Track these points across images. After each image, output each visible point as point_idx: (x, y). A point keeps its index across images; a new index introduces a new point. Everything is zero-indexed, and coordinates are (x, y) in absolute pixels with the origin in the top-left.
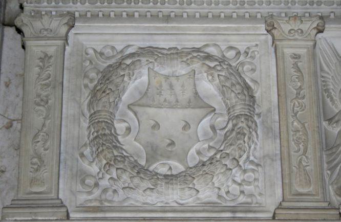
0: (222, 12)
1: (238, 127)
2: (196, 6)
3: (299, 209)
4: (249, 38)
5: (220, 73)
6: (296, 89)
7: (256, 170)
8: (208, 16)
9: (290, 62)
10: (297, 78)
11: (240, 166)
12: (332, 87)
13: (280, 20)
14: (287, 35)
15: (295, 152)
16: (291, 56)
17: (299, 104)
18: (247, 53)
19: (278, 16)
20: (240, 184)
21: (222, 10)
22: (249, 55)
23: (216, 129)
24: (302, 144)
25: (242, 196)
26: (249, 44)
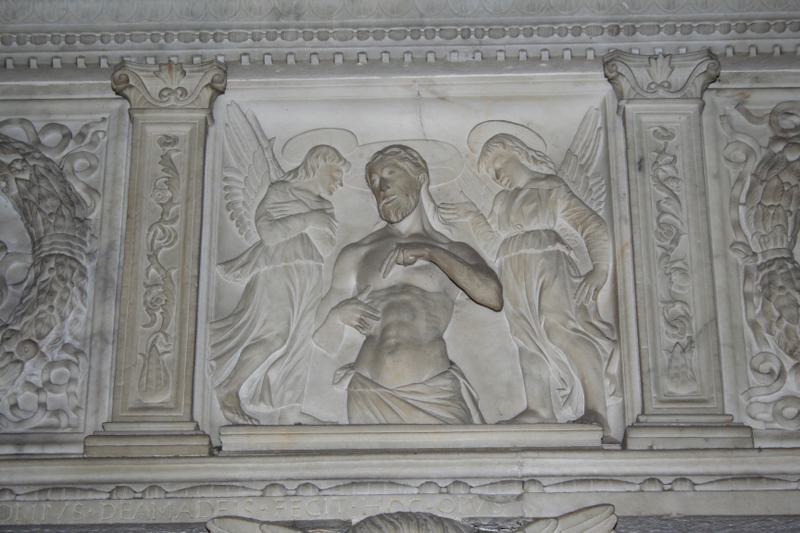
1: (43, 279)
2: (336, 42)
3: (134, 436)
5: (20, 176)
6: (162, 205)
7: (74, 363)
8: (586, 57)
9: (153, 151)
10: (165, 182)
11: (43, 355)
12: (242, 198)
13: (142, 71)
14: (157, 101)
15: (144, 326)
16: (159, 141)
17: (164, 231)
18: (82, 135)
19: (140, 64)
20: (38, 390)
21: (569, 46)
22: (87, 140)
23: (8, 283)
24: (161, 310)
25: (40, 413)
26: (89, 118)
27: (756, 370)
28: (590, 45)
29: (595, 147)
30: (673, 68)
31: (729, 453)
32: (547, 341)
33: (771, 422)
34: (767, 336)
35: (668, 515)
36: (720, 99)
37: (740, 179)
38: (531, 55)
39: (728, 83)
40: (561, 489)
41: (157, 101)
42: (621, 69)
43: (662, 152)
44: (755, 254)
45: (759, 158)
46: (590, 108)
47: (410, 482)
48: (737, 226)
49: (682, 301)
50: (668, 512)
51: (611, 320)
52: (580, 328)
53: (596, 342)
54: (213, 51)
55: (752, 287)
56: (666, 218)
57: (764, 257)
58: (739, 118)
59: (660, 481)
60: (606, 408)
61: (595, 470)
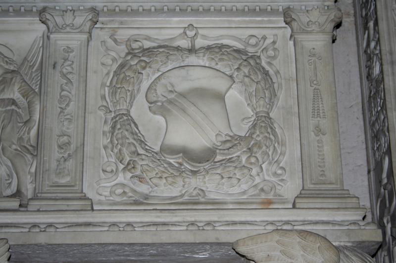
0: (212, 6)
4: (274, 30)
8: (32, 10)
14: (305, 27)
21: (23, 4)
27: (104, 171)
28: (34, 4)
29: (38, 56)
30: (75, 17)
31: (77, 212)
32: (3, 156)
33: (109, 197)
34: (111, 153)
35: (40, 244)
36: (101, 33)
37: (108, 74)
38: (145, 8)
39: (107, 25)
40: (66, 230)
41: (305, 27)
42: (48, 16)
43: (66, 60)
44: (111, 111)
45: (119, 63)
46: (37, 37)
47: (25, 226)
48: (103, 97)
49: (68, 135)
50: (40, 242)
51: (35, 145)
52: (19, 149)
53: (25, 155)
54: (219, 4)
55: (107, 128)
56: (64, 93)
57: (115, 113)
58: (110, 42)
59: (117, 226)
60: (27, 190)
61: (9, 221)
